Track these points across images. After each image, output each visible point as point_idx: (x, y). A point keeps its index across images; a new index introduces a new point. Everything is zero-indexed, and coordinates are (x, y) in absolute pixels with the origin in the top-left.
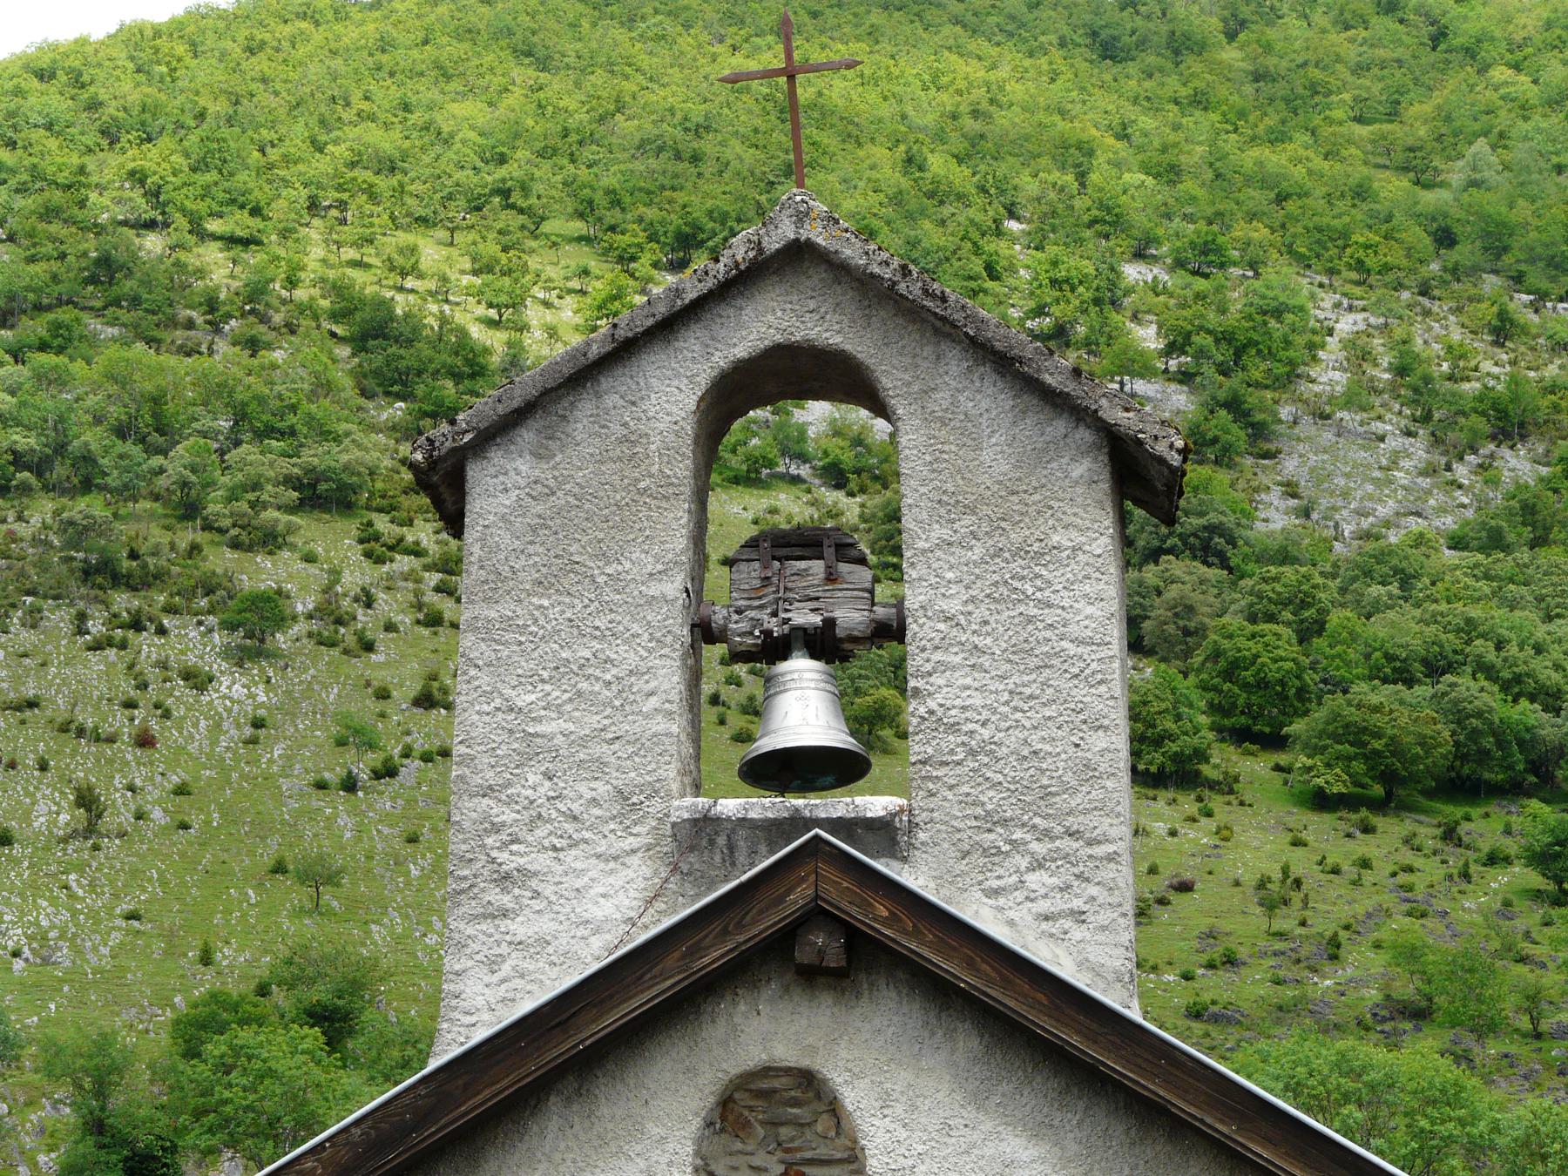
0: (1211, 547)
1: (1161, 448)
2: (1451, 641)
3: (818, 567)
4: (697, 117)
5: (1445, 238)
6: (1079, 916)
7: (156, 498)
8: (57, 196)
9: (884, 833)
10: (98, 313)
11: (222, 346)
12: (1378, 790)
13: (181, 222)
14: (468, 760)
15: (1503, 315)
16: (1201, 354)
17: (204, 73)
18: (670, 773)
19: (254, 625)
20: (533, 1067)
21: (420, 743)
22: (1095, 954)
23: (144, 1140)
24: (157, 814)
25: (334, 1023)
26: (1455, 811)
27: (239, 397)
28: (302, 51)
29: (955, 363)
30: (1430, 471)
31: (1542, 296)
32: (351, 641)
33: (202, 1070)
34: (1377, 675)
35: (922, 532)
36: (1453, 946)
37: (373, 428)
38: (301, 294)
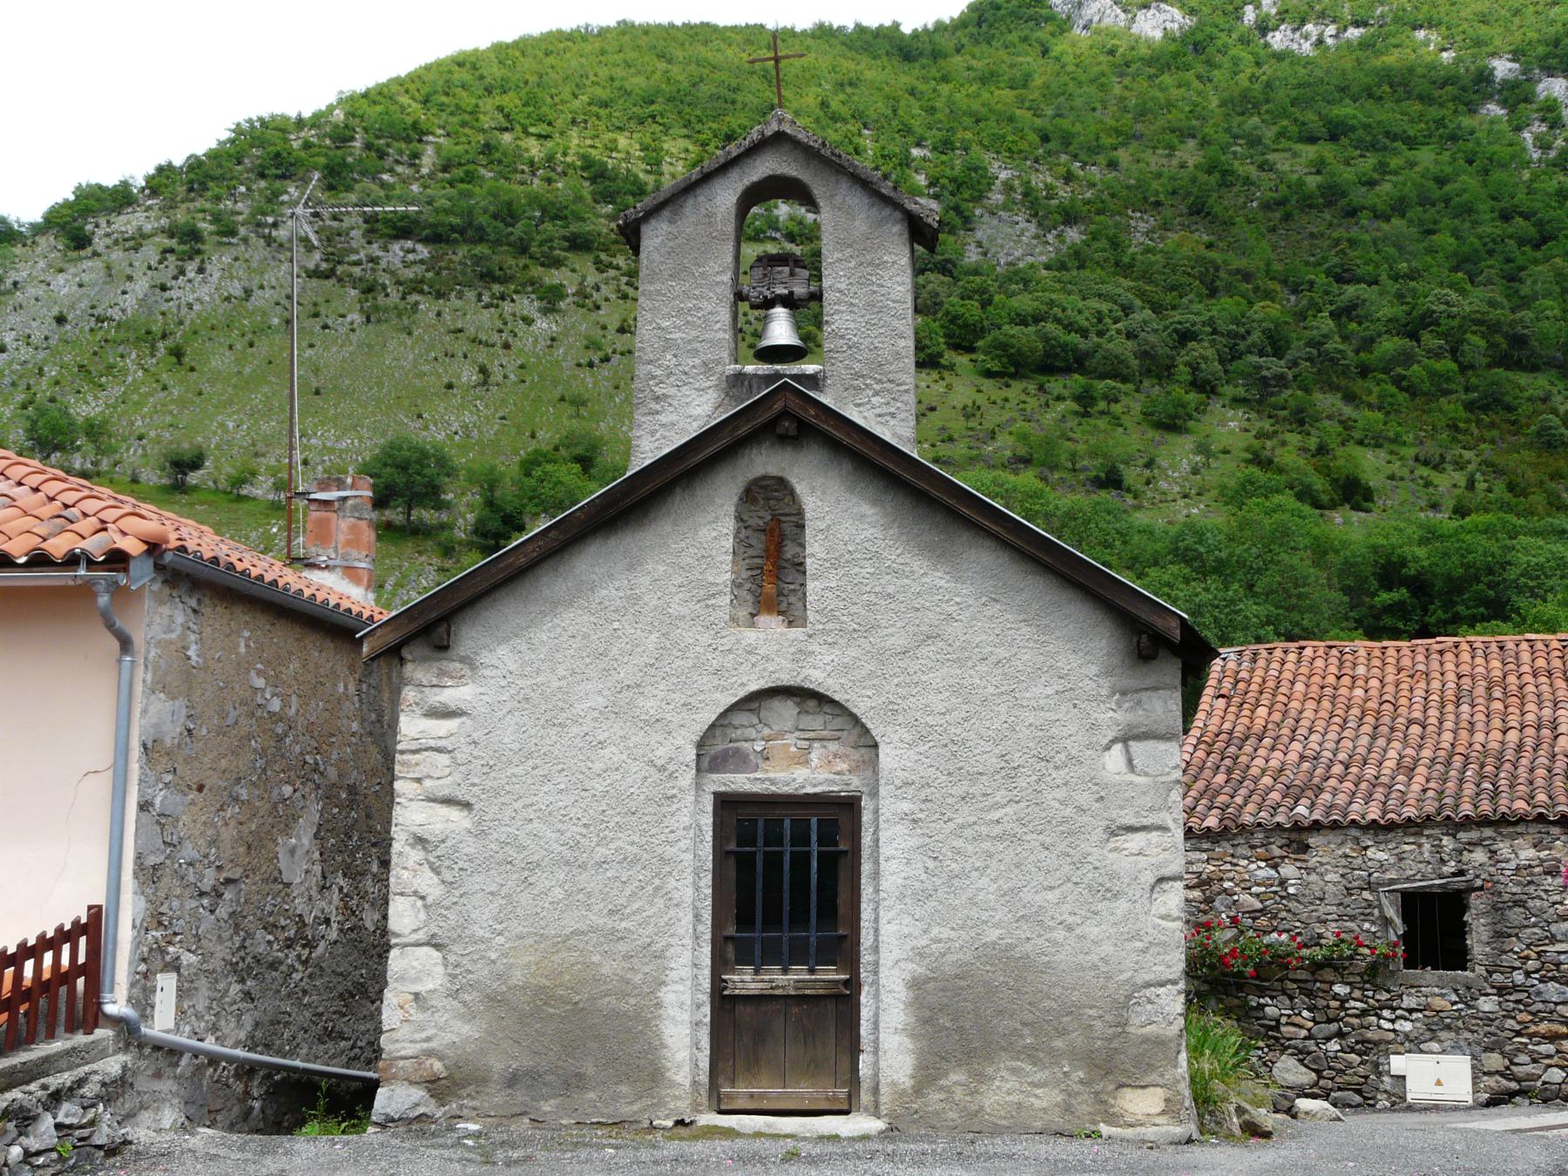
0: (946, 268)
1: (930, 220)
2: (1044, 308)
3: (786, 270)
4: (734, 85)
5: (1045, 139)
6: (893, 415)
7: (509, 245)
8: (467, 117)
9: (813, 381)
10: (485, 166)
11: (536, 181)
12: (1012, 369)
13: (518, 128)
14: (641, 349)
15: (1069, 172)
16: (943, 187)
17: (527, 64)
18: (725, 354)
19: (551, 299)
20: (670, 475)
21: (619, 349)
22: (899, 431)
23: (509, 509)
24: (512, 376)
25: (585, 462)
26: (1043, 379)
27: (544, 202)
28: (568, 55)
29: (845, 184)
30: (1037, 237)
31: (1085, 164)
32: (591, 305)
33: (533, 482)
34: (1012, 322)
35: (830, 256)
36: (1042, 434)
37: (600, 216)
38: (569, 159)
